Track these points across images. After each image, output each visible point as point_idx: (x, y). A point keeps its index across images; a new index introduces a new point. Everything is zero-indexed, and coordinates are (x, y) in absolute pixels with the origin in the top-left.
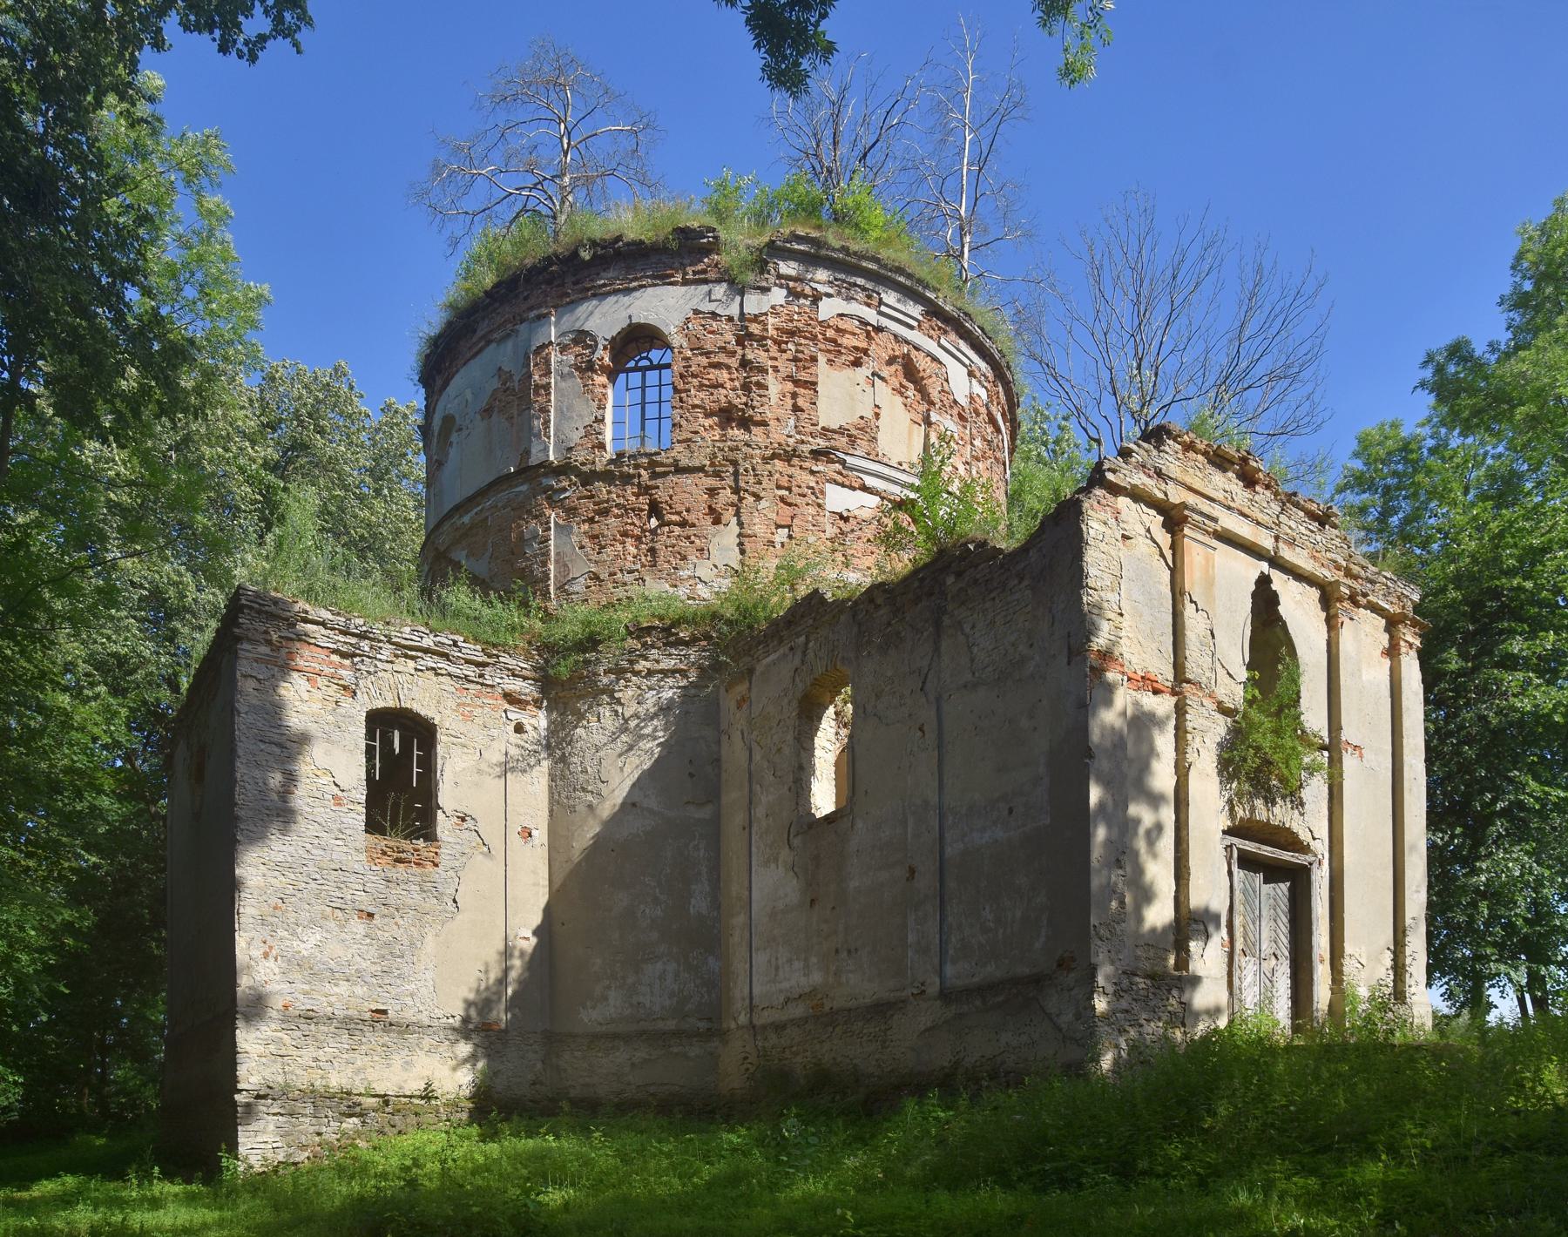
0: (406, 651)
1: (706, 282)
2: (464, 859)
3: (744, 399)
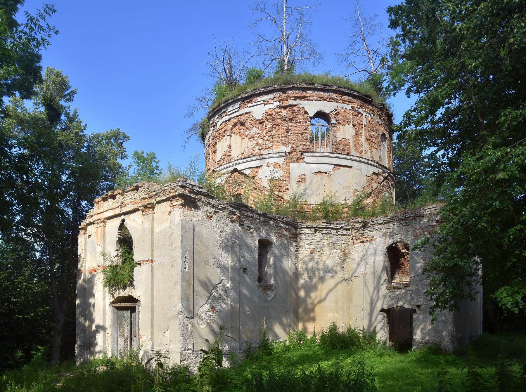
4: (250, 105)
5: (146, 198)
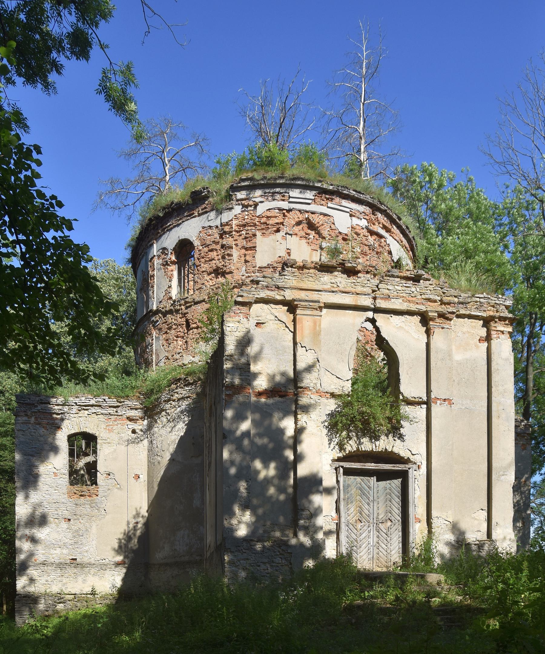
0: (84, 407)
1: (206, 212)
2: (109, 492)
3: (223, 263)
4: (330, 205)
5: (435, 301)
